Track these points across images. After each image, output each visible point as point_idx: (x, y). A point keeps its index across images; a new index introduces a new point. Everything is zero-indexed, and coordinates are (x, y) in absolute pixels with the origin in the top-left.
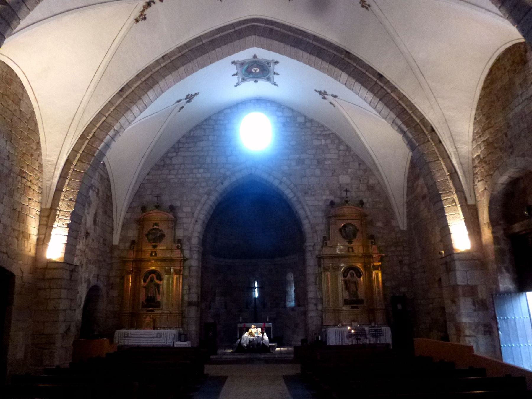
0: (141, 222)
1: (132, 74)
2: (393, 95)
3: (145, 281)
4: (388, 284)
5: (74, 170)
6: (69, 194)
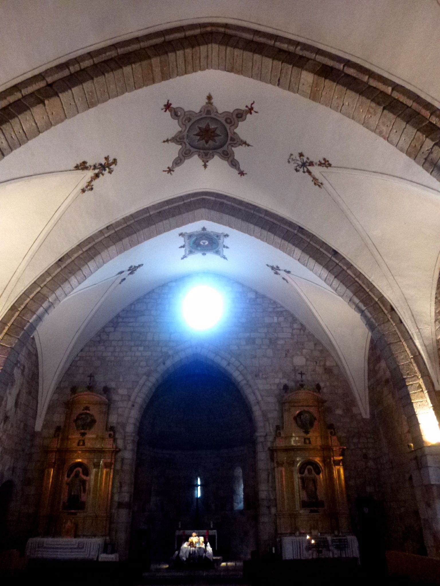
0: (69, 405)
1: (74, 243)
3: (68, 476)
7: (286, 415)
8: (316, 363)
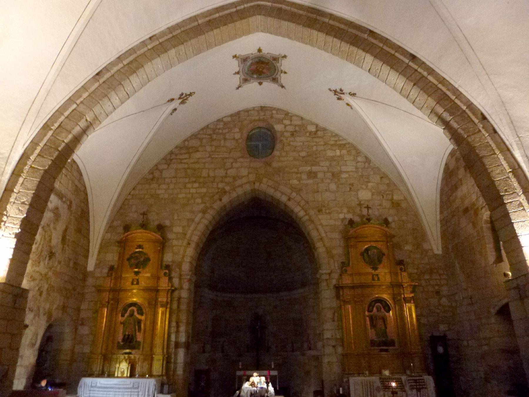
0: (122, 243)
1: (113, 56)
2: (430, 78)
3: (123, 316)
4: (424, 321)
5: (31, 167)
6: (23, 196)
7: (352, 251)
8: (383, 197)
